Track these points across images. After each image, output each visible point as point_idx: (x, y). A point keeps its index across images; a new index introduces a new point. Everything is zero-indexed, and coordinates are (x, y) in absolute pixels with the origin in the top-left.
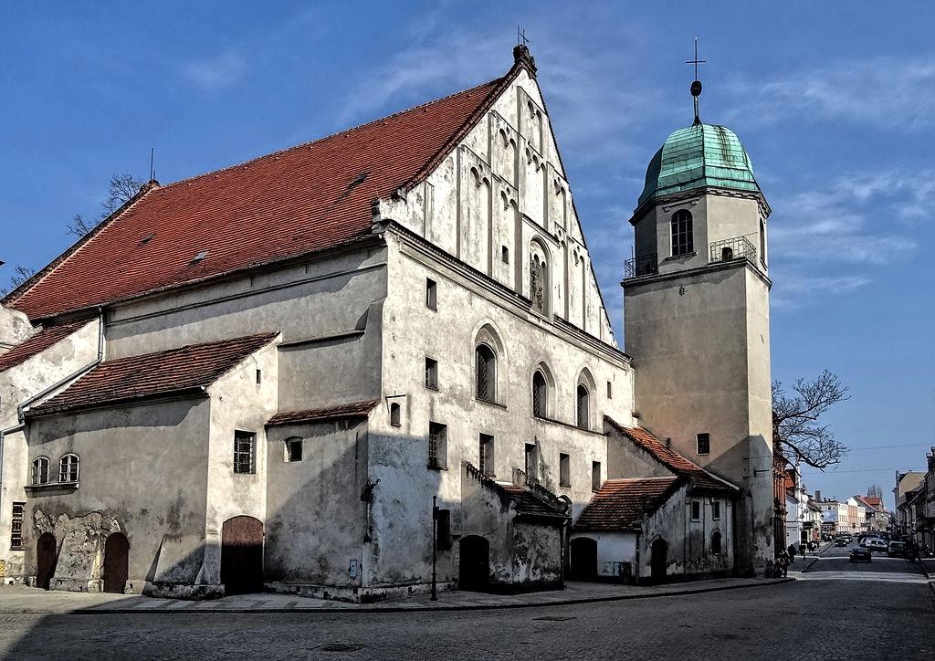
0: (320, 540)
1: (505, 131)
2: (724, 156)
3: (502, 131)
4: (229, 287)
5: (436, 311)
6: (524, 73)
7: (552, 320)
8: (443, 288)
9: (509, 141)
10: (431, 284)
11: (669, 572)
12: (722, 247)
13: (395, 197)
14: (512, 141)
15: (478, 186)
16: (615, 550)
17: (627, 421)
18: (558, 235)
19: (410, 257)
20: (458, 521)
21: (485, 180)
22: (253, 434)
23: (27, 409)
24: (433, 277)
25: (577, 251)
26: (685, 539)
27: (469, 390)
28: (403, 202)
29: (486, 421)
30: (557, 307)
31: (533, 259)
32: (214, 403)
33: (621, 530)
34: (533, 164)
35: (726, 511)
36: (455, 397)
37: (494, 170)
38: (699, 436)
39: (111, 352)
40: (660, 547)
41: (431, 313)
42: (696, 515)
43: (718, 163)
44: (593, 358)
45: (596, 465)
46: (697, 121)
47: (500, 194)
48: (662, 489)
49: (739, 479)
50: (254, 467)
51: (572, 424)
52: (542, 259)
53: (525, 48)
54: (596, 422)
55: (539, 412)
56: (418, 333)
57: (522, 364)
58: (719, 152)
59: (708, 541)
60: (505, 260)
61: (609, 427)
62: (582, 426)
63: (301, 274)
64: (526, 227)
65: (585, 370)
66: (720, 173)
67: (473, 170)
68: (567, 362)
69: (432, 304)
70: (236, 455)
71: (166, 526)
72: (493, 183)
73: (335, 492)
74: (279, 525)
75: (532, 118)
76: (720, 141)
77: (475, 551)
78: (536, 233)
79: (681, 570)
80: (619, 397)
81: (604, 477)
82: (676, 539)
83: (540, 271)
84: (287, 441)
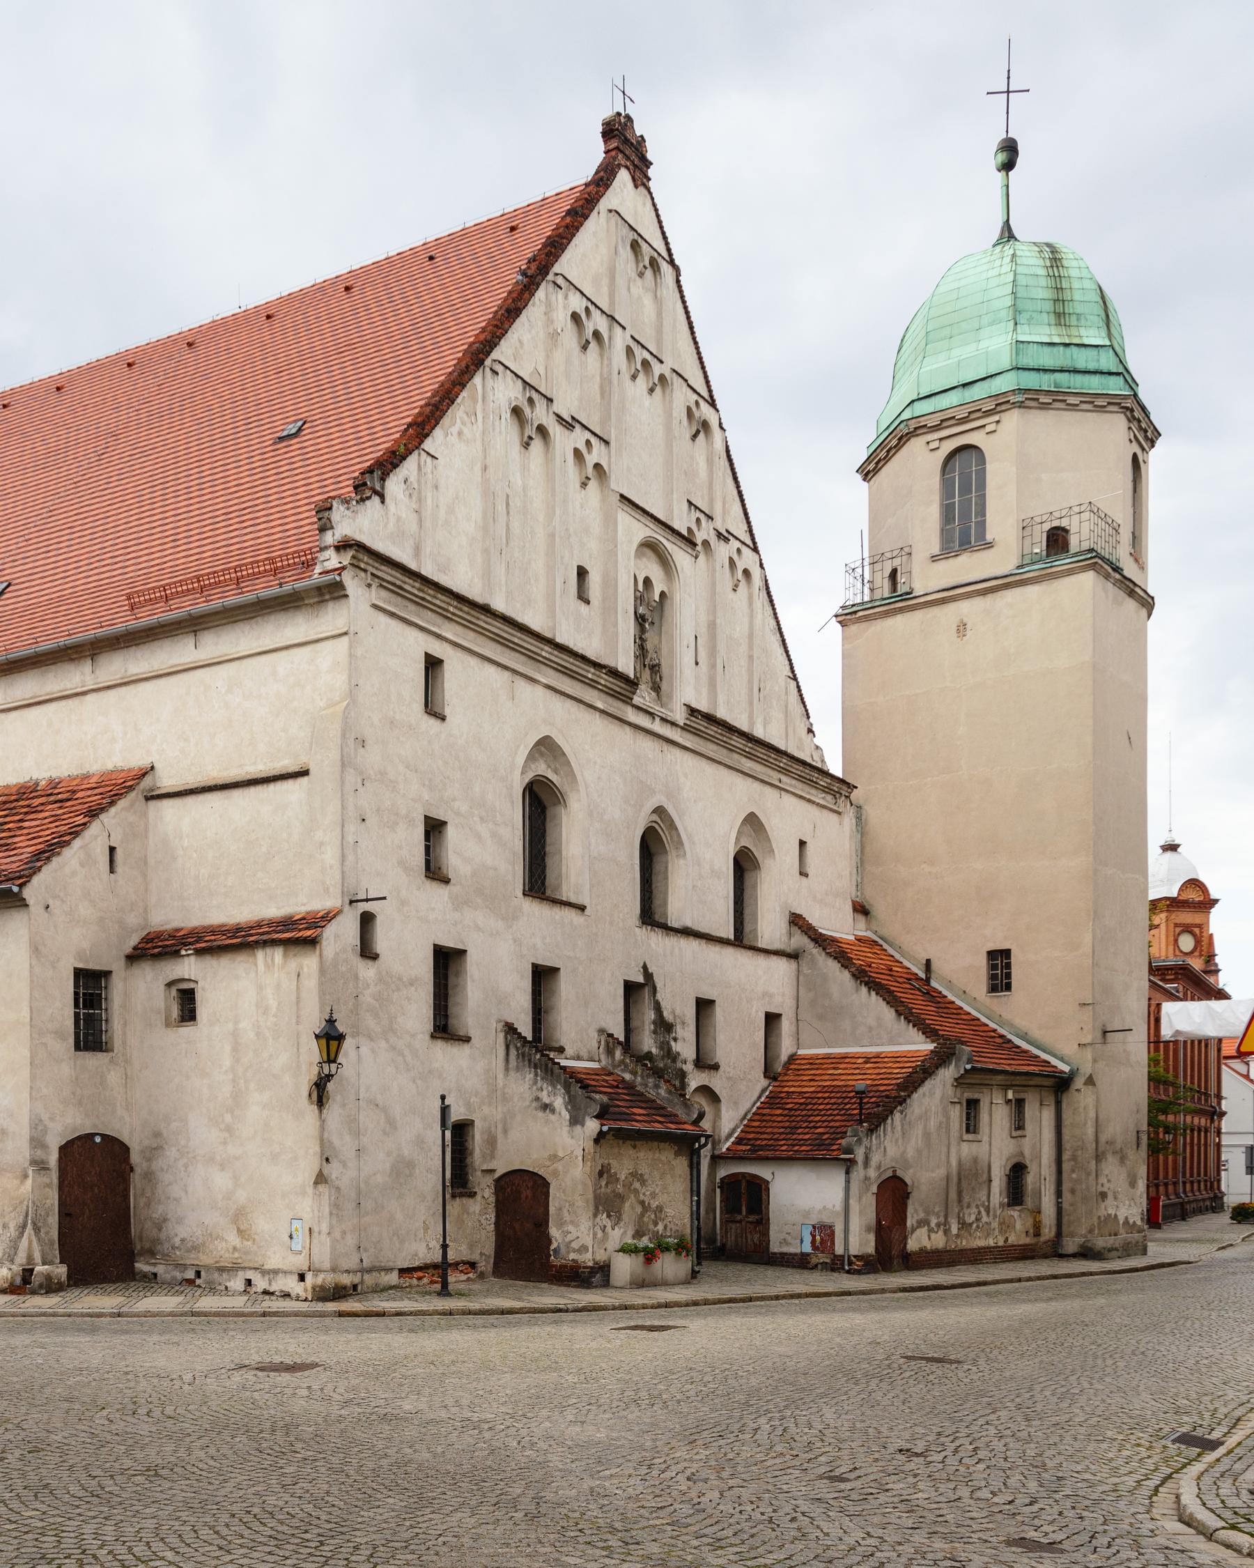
0: (236, 1178)
4: (51, 675)
5: (443, 719)
7: (680, 716)
8: (456, 669)
9: (590, 337)
10: (433, 664)
11: (913, 1245)
12: (1047, 527)
14: (597, 335)
16: (805, 1197)
17: (838, 922)
18: (694, 528)
20: (492, 1142)
22: (107, 974)
24: (438, 649)
26: (948, 1178)
27: (510, 877)
29: (544, 938)
30: (688, 689)
31: (641, 587)
33: (824, 1152)
37: (558, 407)
38: (992, 955)
42: (971, 1125)
45: (772, 1019)
51: (723, 935)
52: (658, 587)
53: (628, 118)
54: (770, 926)
56: (407, 767)
58: (1048, 306)
62: (741, 939)
66: (1048, 358)
67: (516, 411)
68: (711, 806)
70: (77, 1015)
72: (555, 430)
75: (641, 275)
76: (1051, 282)
78: (649, 533)
79: (938, 1241)
81: (786, 1047)
82: (926, 1179)
83: (650, 613)
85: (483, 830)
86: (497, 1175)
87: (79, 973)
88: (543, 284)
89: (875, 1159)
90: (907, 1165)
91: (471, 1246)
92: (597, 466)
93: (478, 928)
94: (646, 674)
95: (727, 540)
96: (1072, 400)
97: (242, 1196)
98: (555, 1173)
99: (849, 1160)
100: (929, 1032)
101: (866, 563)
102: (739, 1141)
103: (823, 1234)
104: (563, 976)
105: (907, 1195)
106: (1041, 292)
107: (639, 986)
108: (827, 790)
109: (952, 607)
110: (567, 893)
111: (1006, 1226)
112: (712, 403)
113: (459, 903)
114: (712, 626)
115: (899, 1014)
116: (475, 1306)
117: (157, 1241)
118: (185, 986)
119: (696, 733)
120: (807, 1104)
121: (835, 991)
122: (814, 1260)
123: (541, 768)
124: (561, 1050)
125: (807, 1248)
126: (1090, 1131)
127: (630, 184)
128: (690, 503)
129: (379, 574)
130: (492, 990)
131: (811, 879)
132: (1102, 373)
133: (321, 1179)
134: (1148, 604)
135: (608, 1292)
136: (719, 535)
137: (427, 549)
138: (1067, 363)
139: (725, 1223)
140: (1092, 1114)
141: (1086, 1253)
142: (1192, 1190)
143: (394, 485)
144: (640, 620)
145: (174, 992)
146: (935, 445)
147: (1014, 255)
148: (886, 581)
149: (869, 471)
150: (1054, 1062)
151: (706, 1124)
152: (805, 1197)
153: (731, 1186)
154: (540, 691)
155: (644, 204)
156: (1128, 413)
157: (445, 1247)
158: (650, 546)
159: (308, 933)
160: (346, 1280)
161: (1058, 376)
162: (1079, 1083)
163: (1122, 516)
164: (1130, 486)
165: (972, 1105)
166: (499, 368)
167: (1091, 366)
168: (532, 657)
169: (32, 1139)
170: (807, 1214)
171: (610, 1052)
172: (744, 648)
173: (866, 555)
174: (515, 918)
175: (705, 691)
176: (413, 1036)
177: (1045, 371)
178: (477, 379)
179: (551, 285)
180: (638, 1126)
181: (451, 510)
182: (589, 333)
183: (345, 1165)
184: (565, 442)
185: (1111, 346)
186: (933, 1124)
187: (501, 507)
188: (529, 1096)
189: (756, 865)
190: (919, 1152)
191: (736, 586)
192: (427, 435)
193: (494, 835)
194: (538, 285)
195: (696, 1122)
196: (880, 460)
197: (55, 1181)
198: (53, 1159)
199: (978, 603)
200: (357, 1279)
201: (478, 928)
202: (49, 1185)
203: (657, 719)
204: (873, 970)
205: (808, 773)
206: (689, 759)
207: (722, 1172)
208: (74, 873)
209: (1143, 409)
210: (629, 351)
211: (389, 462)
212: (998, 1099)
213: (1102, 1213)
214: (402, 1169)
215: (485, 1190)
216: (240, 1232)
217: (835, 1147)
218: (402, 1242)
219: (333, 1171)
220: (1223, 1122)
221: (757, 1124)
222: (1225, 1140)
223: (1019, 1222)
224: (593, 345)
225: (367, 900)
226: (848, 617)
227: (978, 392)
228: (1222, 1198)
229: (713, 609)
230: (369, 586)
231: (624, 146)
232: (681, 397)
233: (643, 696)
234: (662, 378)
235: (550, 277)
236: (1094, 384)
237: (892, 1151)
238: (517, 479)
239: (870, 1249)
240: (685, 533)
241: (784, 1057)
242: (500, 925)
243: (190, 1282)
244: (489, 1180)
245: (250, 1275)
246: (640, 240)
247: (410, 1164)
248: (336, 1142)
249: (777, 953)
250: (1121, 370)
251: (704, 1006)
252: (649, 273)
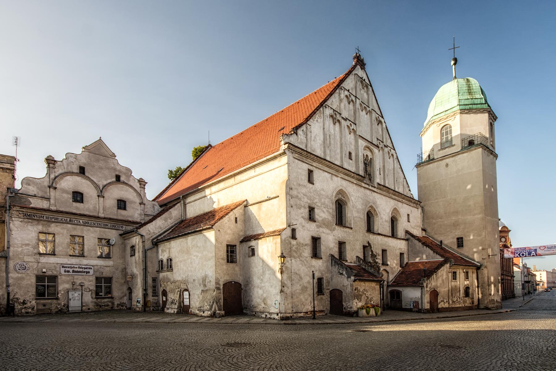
0: (263, 291)
2: (469, 93)
5: (313, 184)
6: (358, 67)
7: (376, 185)
10: (310, 172)
11: (440, 306)
12: (469, 140)
14: (352, 101)
17: (418, 232)
19: (299, 160)
20: (328, 282)
22: (235, 246)
23: (155, 240)
30: (378, 179)
34: (364, 111)
35: (473, 276)
36: (325, 224)
37: (343, 116)
38: (458, 239)
40: (435, 294)
41: (311, 185)
44: (399, 203)
47: (346, 127)
48: (435, 266)
50: (236, 261)
54: (401, 233)
55: (370, 229)
57: (360, 207)
58: (467, 91)
59: (462, 291)
60: (350, 158)
61: (408, 236)
62: (393, 235)
64: (361, 141)
65: (395, 209)
68: (385, 207)
69: (310, 180)
71: (202, 286)
73: (268, 270)
77: (336, 297)
79: (446, 305)
81: (406, 260)
82: (443, 290)
83: (368, 163)
85: (325, 210)
89: (429, 286)
90: (437, 287)
91: (323, 307)
92: (353, 129)
93: (324, 233)
94: (367, 176)
97: (265, 295)
98: (344, 290)
100: (442, 256)
102: (394, 282)
103: (416, 303)
105: (438, 295)
106: (465, 88)
107: (367, 247)
108: (414, 203)
109: (444, 161)
110: (347, 225)
111: (464, 302)
113: (318, 227)
114: (384, 166)
115: (434, 252)
116: (320, 322)
117: (247, 306)
119: (380, 189)
121: (418, 247)
122: (414, 310)
125: (412, 307)
126: (486, 279)
127: (360, 69)
131: (412, 221)
133: (282, 291)
134: (496, 156)
135: (357, 318)
136: (385, 146)
137: (309, 145)
139: (391, 301)
140: (487, 275)
141: (487, 308)
143: (300, 132)
144: (365, 164)
152: (411, 294)
153: (392, 292)
154: (339, 179)
157: (314, 307)
160: (289, 315)
162: (482, 268)
165: (455, 273)
168: (337, 171)
169: (216, 283)
170: (411, 299)
171: (359, 262)
172: (392, 171)
174: (334, 230)
175: (382, 181)
176: (307, 257)
178: (321, 109)
180: (365, 278)
181: (315, 138)
183: (288, 288)
186: (444, 277)
187: (328, 137)
188: (337, 272)
189: (397, 220)
190: (441, 284)
193: (327, 211)
195: (381, 277)
197: (222, 292)
198: (221, 287)
199: (451, 159)
200: (292, 315)
201: (324, 233)
202: (220, 293)
204: (426, 242)
205: (410, 200)
206: (379, 196)
207: (390, 289)
208: (226, 223)
210: (361, 104)
211: (300, 126)
212: (461, 271)
213: (490, 299)
214: (304, 289)
215: (327, 292)
216: (264, 304)
218: (304, 306)
219: (285, 289)
222: (515, 282)
223: (468, 301)
224: (351, 103)
229: (384, 162)
231: (360, 62)
232: (374, 115)
237: (433, 284)
238: (332, 131)
239: (429, 307)
241: (405, 263)
242: (329, 232)
243: (254, 315)
244: (328, 291)
245: (266, 314)
247: (306, 288)
248: (286, 282)
249: (403, 239)
251: (384, 251)
252: (365, 88)
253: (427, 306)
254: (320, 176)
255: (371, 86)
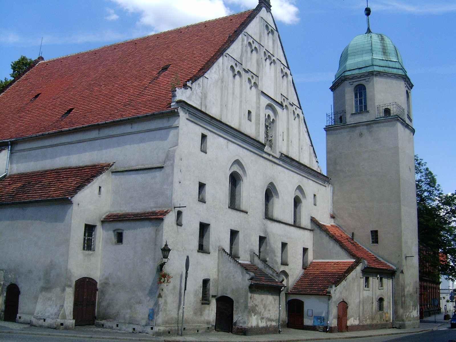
1: (252, 43)
3: (250, 43)
11: (349, 323)
12: (384, 108)
13: (185, 86)
15: (234, 76)
17: (326, 221)
18: (283, 102)
21: (239, 72)
24: (206, 132)
25: (295, 111)
26: (360, 302)
28: (190, 89)
32: (75, 207)
37: (244, 66)
39: (13, 169)
43: (380, 57)
45: (305, 250)
46: (369, 31)
49: (396, 262)
54: (305, 222)
58: (381, 50)
62: (296, 225)
63: (127, 129)
66: (382, 63)
68: (287, 181)
70: (84, 239)
74: (106, 284)
76: (381, 44)
77: (226, 306)
79: (357, 322)
80: (321, 202)
81: (310, 257)
83: (270, 124)
84: (114, 231)
86: (217, 297)
87: (86, 226)
88: (241, 34)
94: (268, 143)
95: (292, 106)
96: (390, 75)
99: (329, 295)
100: (353, 256)
101: (333, 114)
104: (240, 233)
110: (243, 208)
112: (288, 68)
118: (119, 231)
119: (283, 161)
120: (316, 277)
123: (236, 168)
124: (239, 258)
127: (266, 11)
128: (281, 94)
129: (189, 110)
130: (219, 237)
132: (397, 68)
134: (413, 131)
138: (387, 65)
142: (432, 307)
144: (267, 127)
145: (116, 232)
146: (352, 83)
147: (371, 36)
148: (339, 119)
149: (333, 89)
150: (391, 265)
151: (284, 283)
155: (269, 16)
156: (405, 80)
158: (269, 106)
159: (160, 217)
161: (385, 68)
163: (405, 106)
164: (406, 99)
165: (367, 280)
166: (228, 55)
167: (394, 66)
173: (333, 112)
177: (382, 66)
179: (243, 35)
182: (253, 48)
184: (245, 76)
185: (399, 62)
191: (295, 118)
192: (206, 72)
194: (239, 35)
196: (336, 86)
203: (271, 156)
209: (409, 79)
215: (214, 302)
217: (324, 291)
220: (440, 286)
221: (300, 283)
225: (180, 207)
226: (328, 129)
227: (363, 71)
228: (440, 310)
230: (186, 113)
233: (267, 149)
234: (274, 60)
235: (243, 33)
236: (395, 71)
240: (280, 103)
246: (268, 25)
250: (402, 68)
251: (284, 245)
253: (333, 322)
254: (215, 141)
255: (277, 31)
